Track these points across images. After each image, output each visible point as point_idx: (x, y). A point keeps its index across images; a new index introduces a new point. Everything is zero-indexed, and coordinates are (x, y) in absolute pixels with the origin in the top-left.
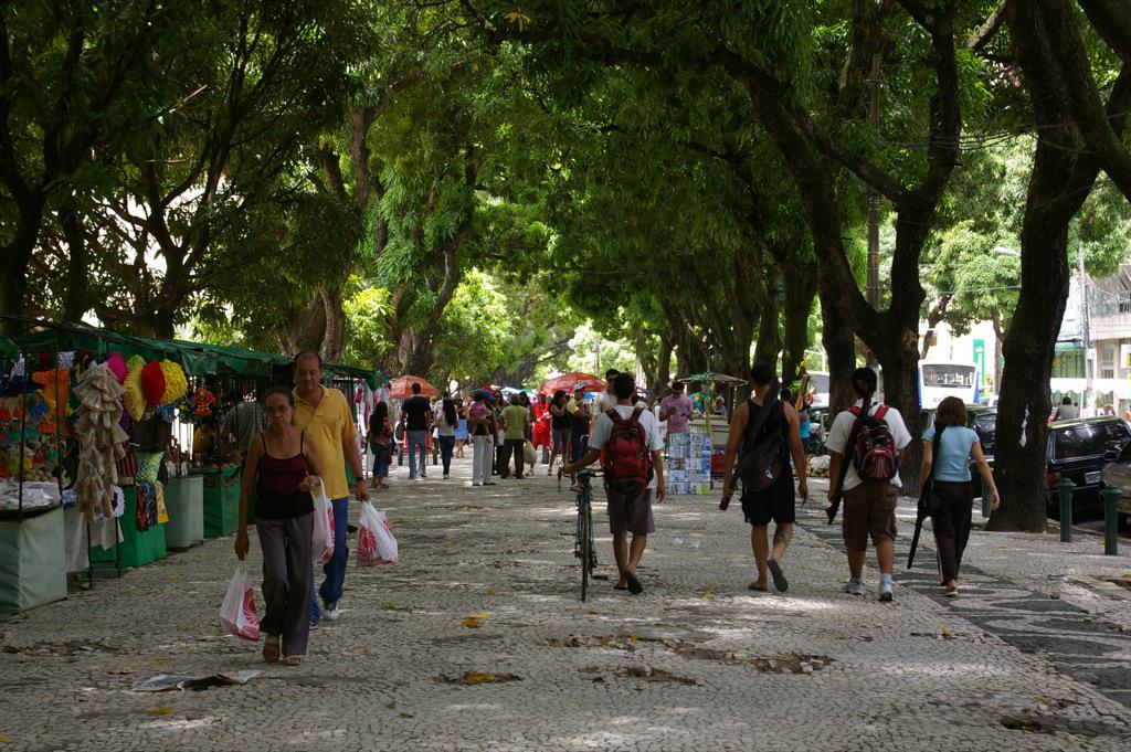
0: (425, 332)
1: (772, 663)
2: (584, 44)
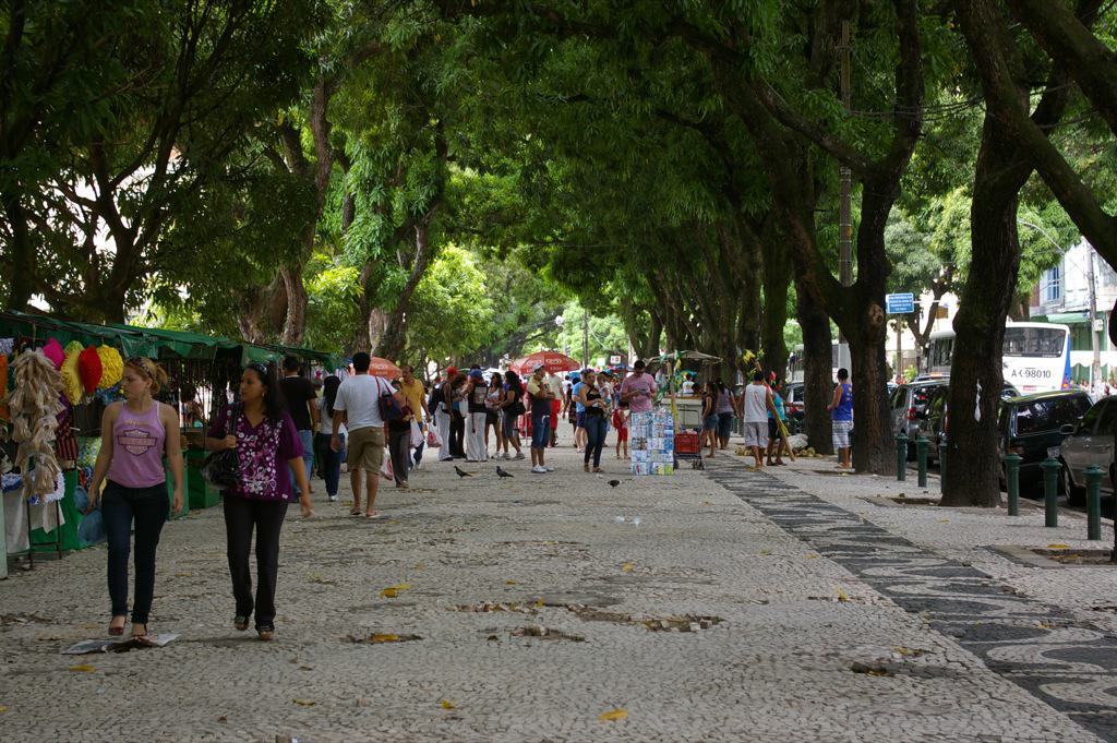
0: (396, 310)
1: (665, 624)
2: (537, 18)
